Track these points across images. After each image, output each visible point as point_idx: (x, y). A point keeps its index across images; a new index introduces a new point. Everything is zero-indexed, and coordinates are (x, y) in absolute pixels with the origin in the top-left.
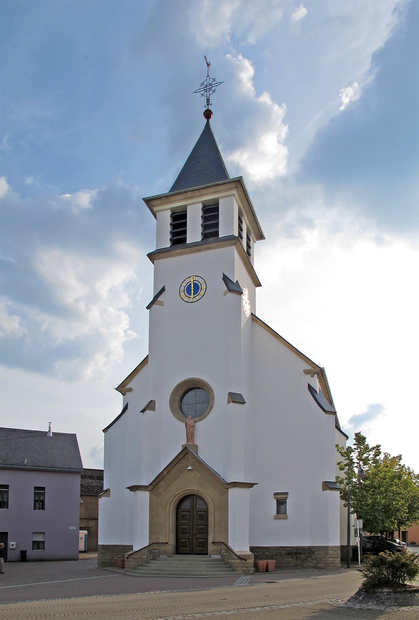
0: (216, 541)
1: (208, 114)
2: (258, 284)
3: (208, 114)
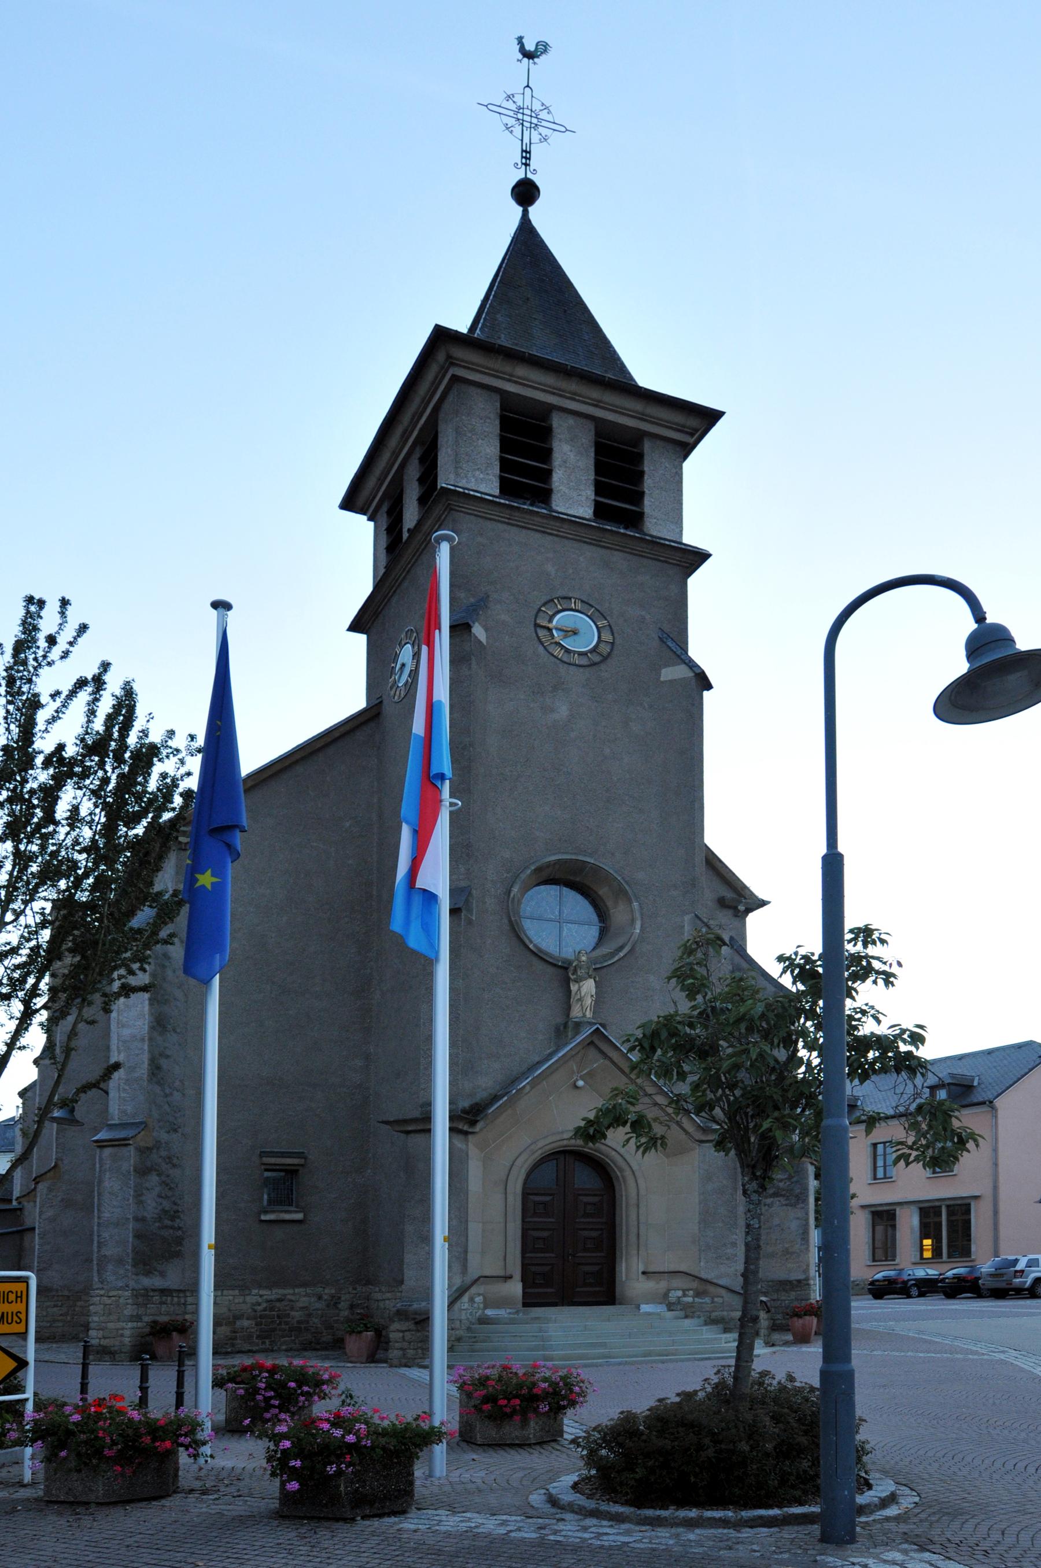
0: (13, 1364)
1: (525, 193)
2: (709, 686)
3: (525, 193)
